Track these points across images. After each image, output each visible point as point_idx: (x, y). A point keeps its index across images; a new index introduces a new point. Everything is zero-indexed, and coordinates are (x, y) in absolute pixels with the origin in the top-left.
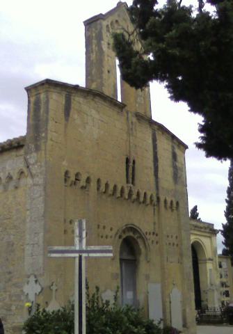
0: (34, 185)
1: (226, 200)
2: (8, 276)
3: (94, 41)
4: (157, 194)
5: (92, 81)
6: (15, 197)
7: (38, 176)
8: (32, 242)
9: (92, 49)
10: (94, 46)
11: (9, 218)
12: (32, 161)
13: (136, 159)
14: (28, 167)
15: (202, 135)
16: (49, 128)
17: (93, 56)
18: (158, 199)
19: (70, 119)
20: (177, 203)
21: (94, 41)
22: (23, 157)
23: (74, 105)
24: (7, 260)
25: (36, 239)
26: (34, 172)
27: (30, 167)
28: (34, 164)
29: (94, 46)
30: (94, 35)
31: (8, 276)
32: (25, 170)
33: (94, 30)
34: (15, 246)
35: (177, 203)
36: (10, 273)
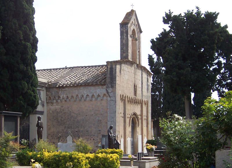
0: (111, 100)
1: (163, 18)
2: (99, 132)
3: (125, 34)
4: (142, 98)
5: (124, 53)
6: (101, 103)
7: (113, 97)
8: (111, 121)
9: (123, 37)
10: (125, 36)
11: (99, 111)
12: (109, 91)
13: (137, 85)
14: (108, 93)
15: (155, 40)
16: (117, 80)
17: (124, 41)
18: (142, 100)
19: (121, 74)
20: (148, 101)
21: (125, 34)
22: (105, 89)
23: (122, 68)
24: (98, 126)
25: (113, 120)
26: (111, 95)
27: (109, 93)
28: (110, 93)
29: (125, 36)
30: (125, 31)
31: (99, 132)
32: (106, 94)
33: (124, 28)
34: (102, 121)
35: (148, 101)
36: (100, 131)
